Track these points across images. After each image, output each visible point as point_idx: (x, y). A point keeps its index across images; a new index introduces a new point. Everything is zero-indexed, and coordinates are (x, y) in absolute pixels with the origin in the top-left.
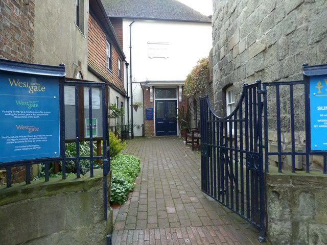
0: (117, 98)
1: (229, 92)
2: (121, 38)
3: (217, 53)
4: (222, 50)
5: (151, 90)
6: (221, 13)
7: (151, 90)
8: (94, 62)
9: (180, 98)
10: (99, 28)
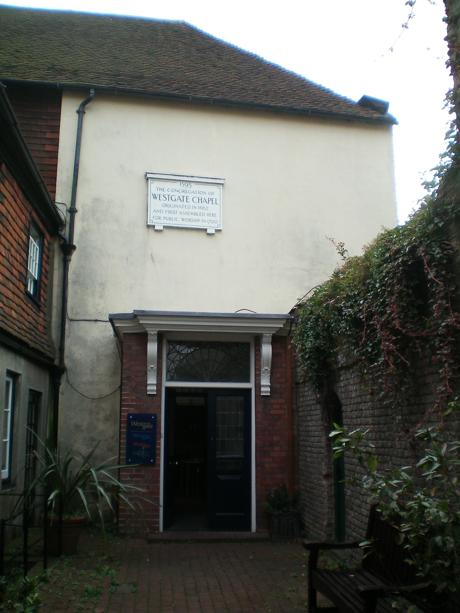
9: (265, 381)
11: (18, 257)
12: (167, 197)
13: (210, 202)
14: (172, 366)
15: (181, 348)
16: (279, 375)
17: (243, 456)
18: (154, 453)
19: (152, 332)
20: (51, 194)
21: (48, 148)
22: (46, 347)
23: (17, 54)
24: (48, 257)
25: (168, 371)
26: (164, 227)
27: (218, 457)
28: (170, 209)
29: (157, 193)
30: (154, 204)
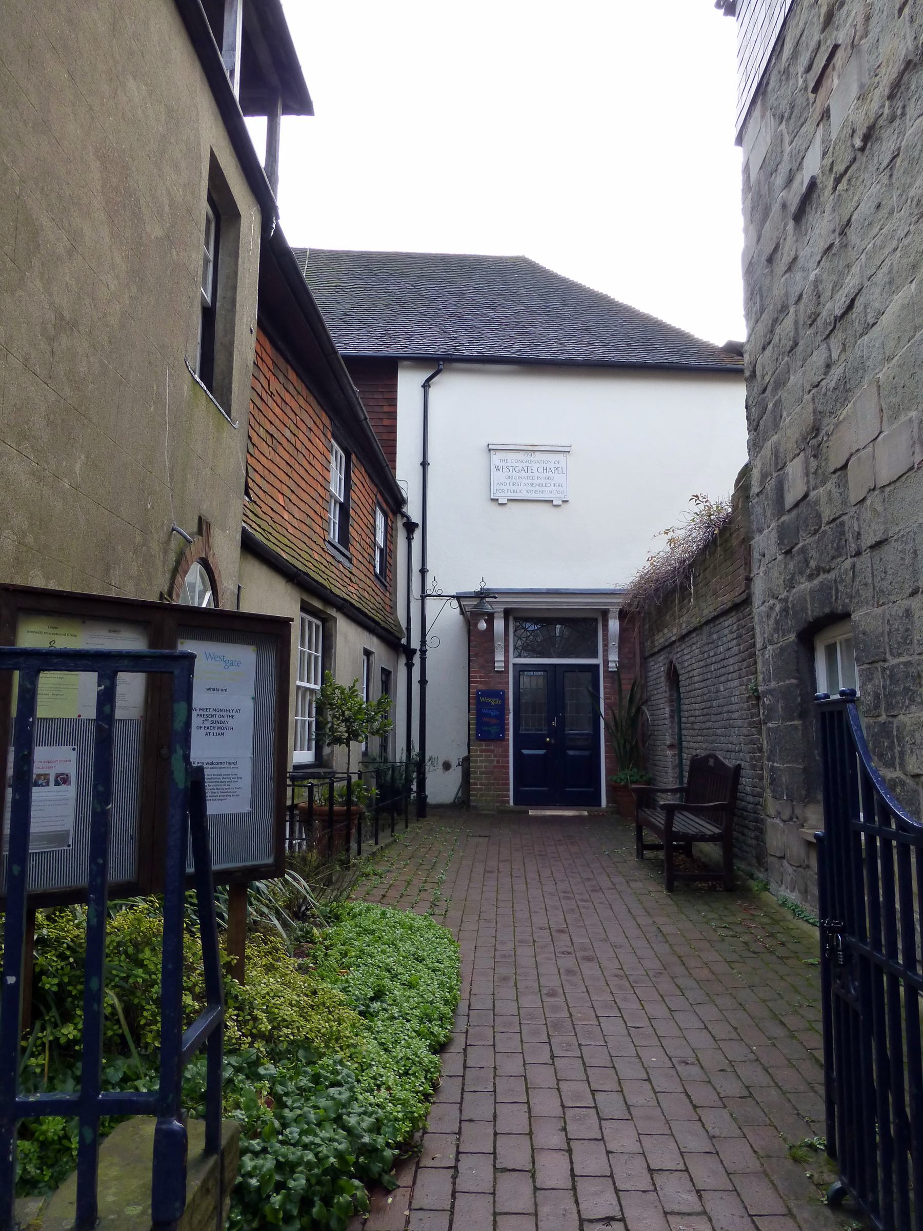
0: (368, 653)
1: (831, 651)
2: (392, 430)
3: (771, 484)
4: (795, 469)
5: (499, 625)
6: (788, 323)
7: (499, 625)
8: (277, 518)
9: (613, 657)
10: (305, 392)
11: (368, 540)
12: (510, 468)
13: (556, 471)
14: (519, 643)
15: (528, 625)
16: (627, 650)
17: (592, 732)
18: (503, 728)
19: (499, 609)
20: (392, 470)
21: (386, 422)
22: (393, 626)
23: (347, 319)
24: (391, 536)
25: (515, 648)
26: (509, 500)
27: (566, 732)
28: (514, 481)
29: (500, 464)
30: (498, 477)
